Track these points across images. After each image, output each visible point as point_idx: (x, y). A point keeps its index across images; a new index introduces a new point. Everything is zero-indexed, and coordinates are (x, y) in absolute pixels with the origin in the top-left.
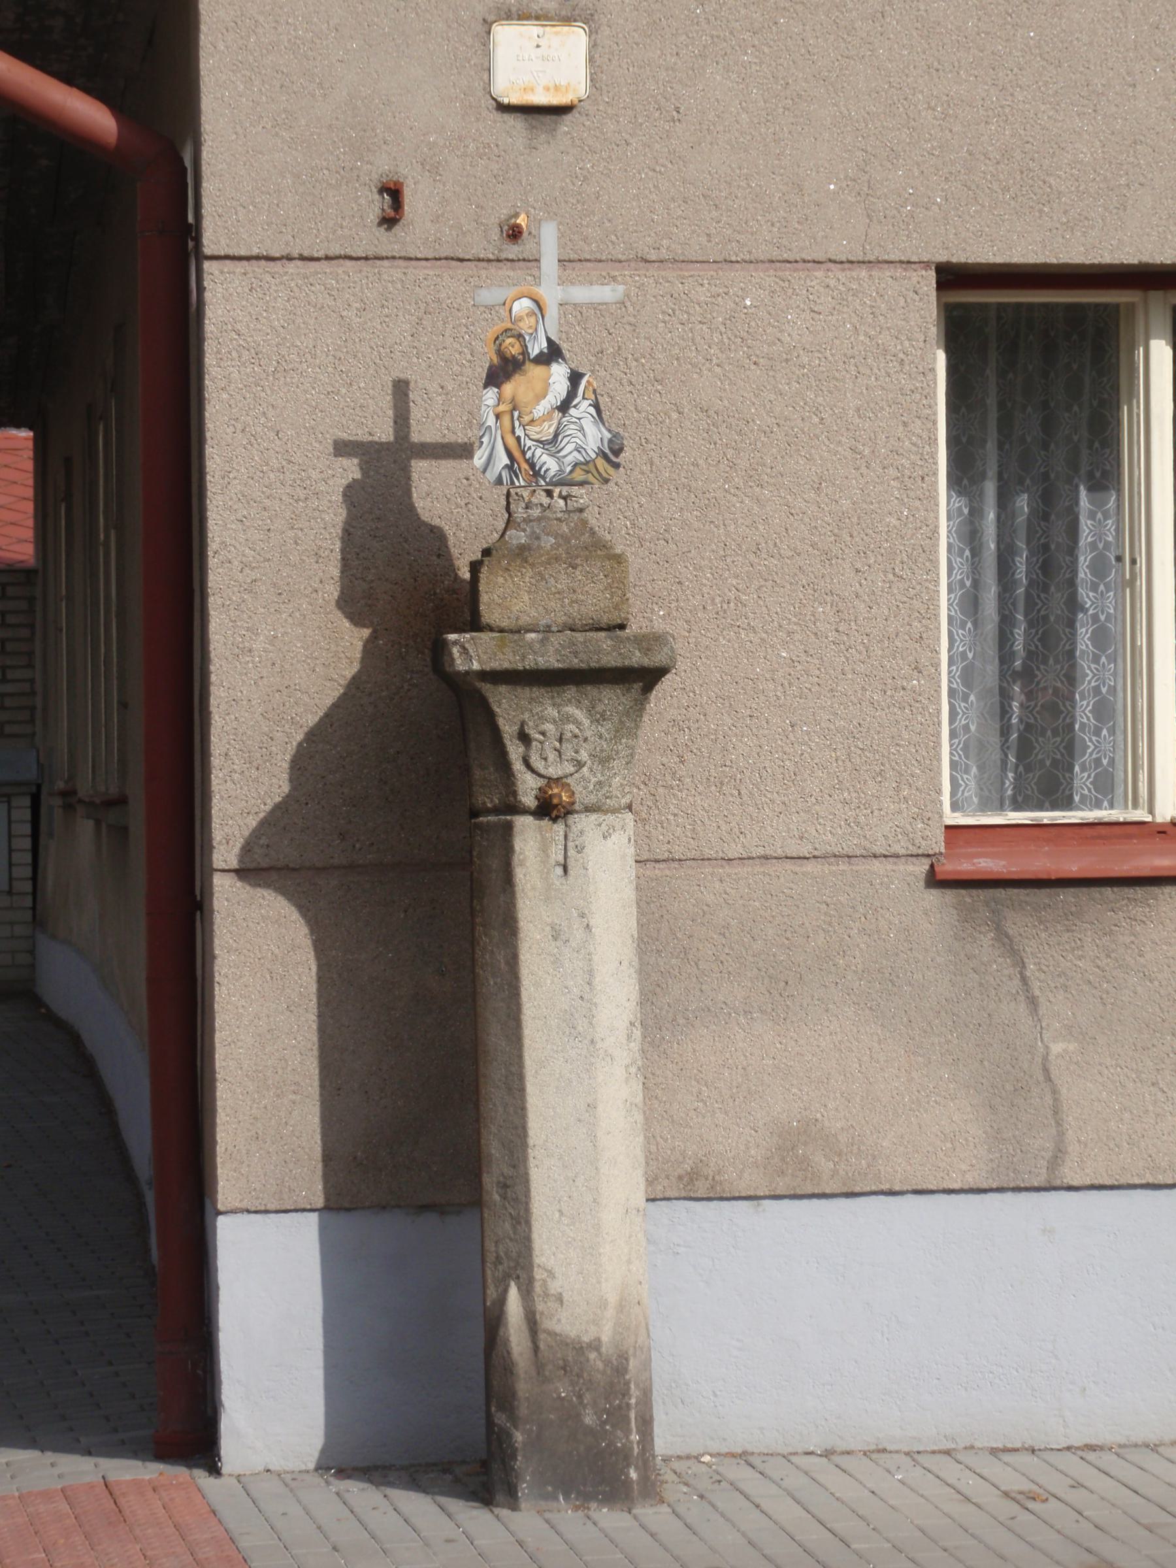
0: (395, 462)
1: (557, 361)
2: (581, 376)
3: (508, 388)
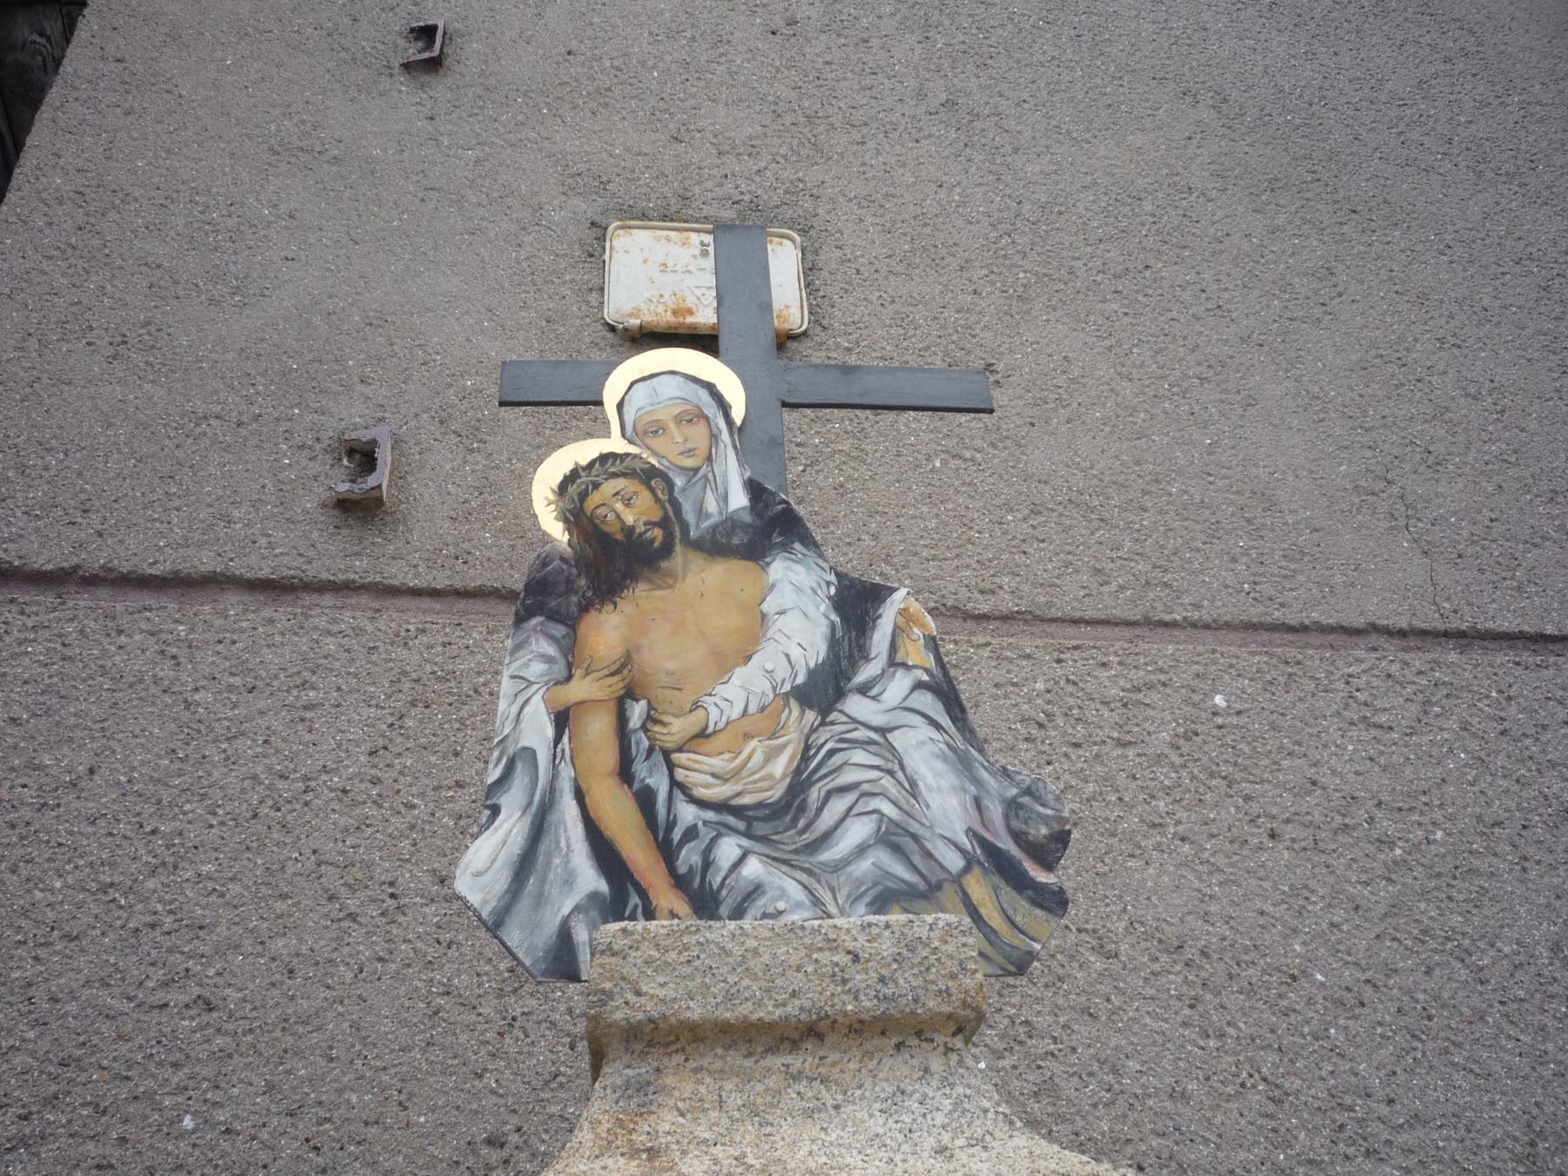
0: (270, 1088)
1: (786, 548)
3: (607, 631)
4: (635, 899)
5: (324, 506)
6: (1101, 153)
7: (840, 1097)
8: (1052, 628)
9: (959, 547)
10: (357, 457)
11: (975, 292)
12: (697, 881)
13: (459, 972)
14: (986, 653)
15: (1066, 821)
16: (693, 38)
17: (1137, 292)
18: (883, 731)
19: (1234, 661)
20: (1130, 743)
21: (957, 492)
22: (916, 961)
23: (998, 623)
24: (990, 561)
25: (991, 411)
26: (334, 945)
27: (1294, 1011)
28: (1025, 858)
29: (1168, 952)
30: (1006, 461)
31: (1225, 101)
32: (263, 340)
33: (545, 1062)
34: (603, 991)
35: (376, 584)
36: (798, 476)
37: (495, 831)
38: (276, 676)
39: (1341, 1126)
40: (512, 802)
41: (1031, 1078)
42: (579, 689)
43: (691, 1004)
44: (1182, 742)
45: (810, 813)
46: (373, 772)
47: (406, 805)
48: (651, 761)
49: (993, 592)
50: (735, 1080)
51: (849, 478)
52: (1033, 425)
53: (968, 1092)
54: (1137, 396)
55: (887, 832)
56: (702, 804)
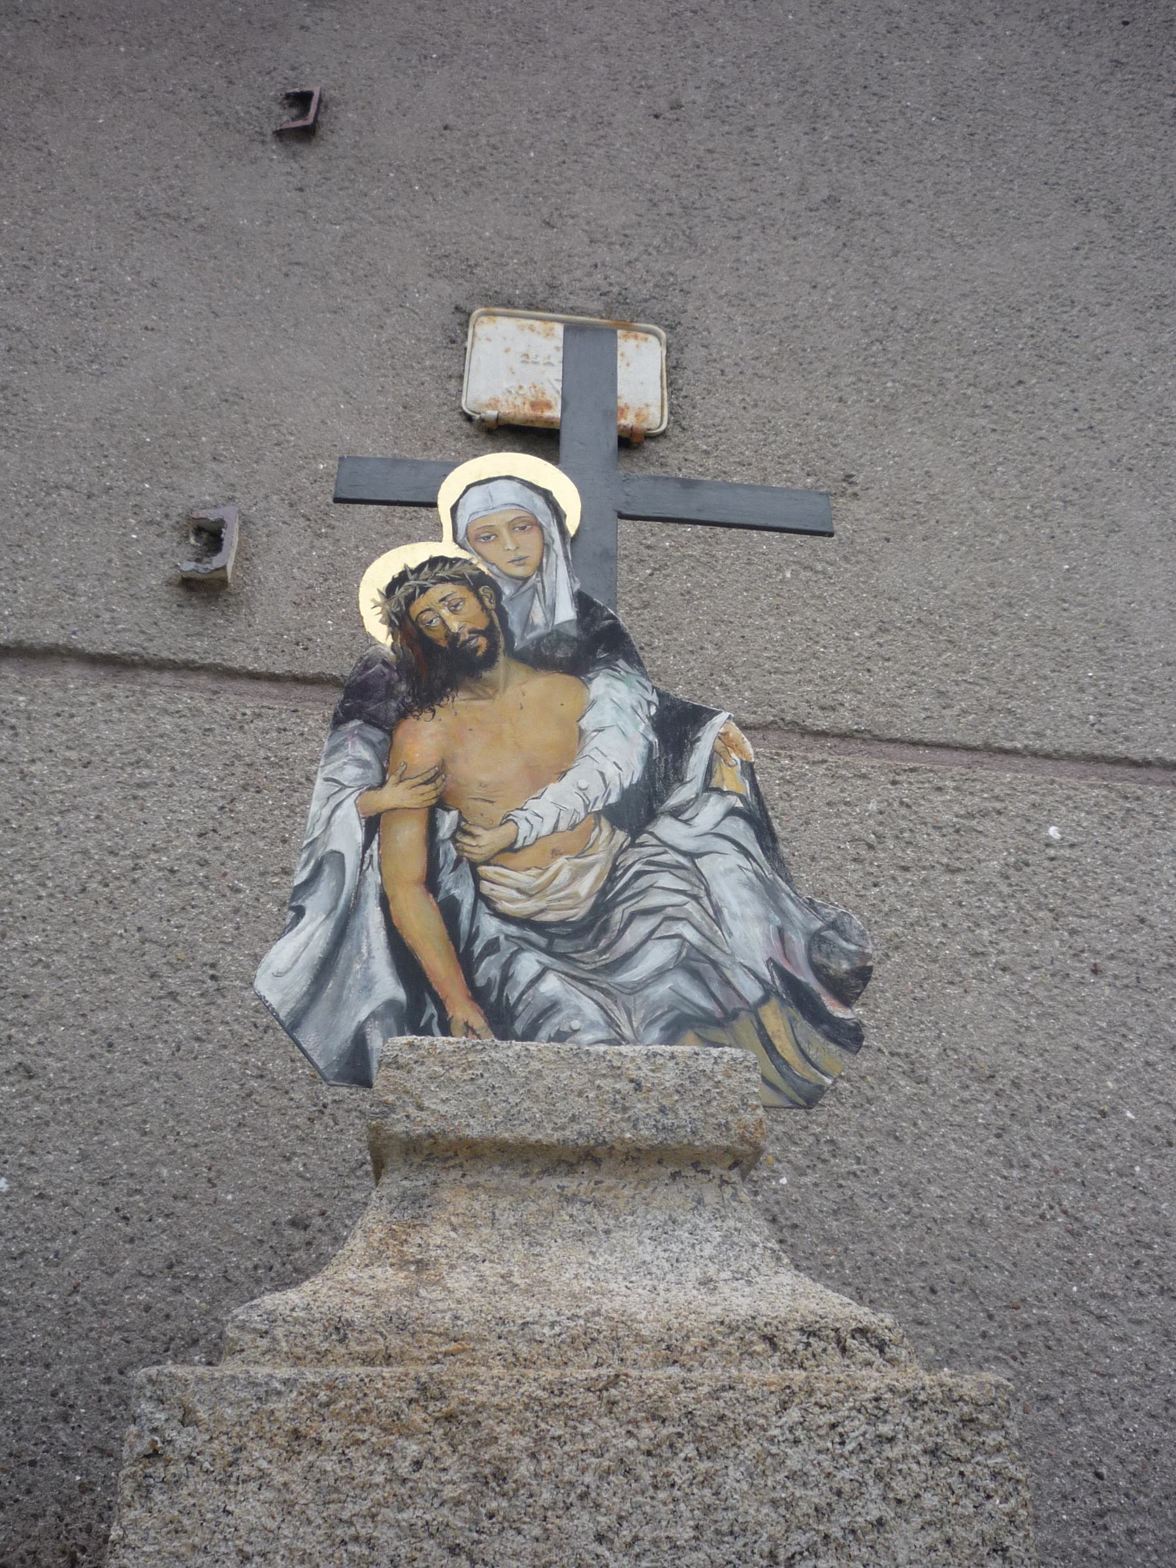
0: (84, 1157)
1: (609, 664)
2: (697, 716)
3: (423, 739)
4: (431, 1010)
5: (168, 584)
6: (984, 260)
7: (612, 1222)
8: (891, 749)
9: (803, 661)
10: (205, 535)
11: (841, 400)
12: (495, 994)
13: (273, 1057)
14: (821, 770)
15: (870, 957)
16: (573, 118)
17: (1007, 407)
18: (692, 856)
19: (1072, 793)
20: (959, 870)
21: (806, 604)
22: (697, 1094)
23: (835, 741)
24: (833, 677)
25: (831, 535)
26: (153, 1022)
27: (1101, 1146)
28: (823, 991)
29: (979, 1080)
30: (858, 576)
31: (1118, 210)
32: (118, 411)
33: (352, 1150)
34: (386, 1103)
35: (216, 666)
36: (646, 580)
37: (298, 933)
38: (111, 753)
39: (1138, 1263)
40: (317, 905)
41: (831, 1196)
42: (392, 796)
43: (472, 1121)
44: (1011, 871)
45: (612, 934)
46: (201, 853)
47: (231, 889)
48: (458, 872)
49: (833, 709)
50: (510, 1198)
51: (697, 585)
52: (888, 540)
53: (739, 1225)
54: (997, 516)
55: (687, 957)
56: (505, 918)
